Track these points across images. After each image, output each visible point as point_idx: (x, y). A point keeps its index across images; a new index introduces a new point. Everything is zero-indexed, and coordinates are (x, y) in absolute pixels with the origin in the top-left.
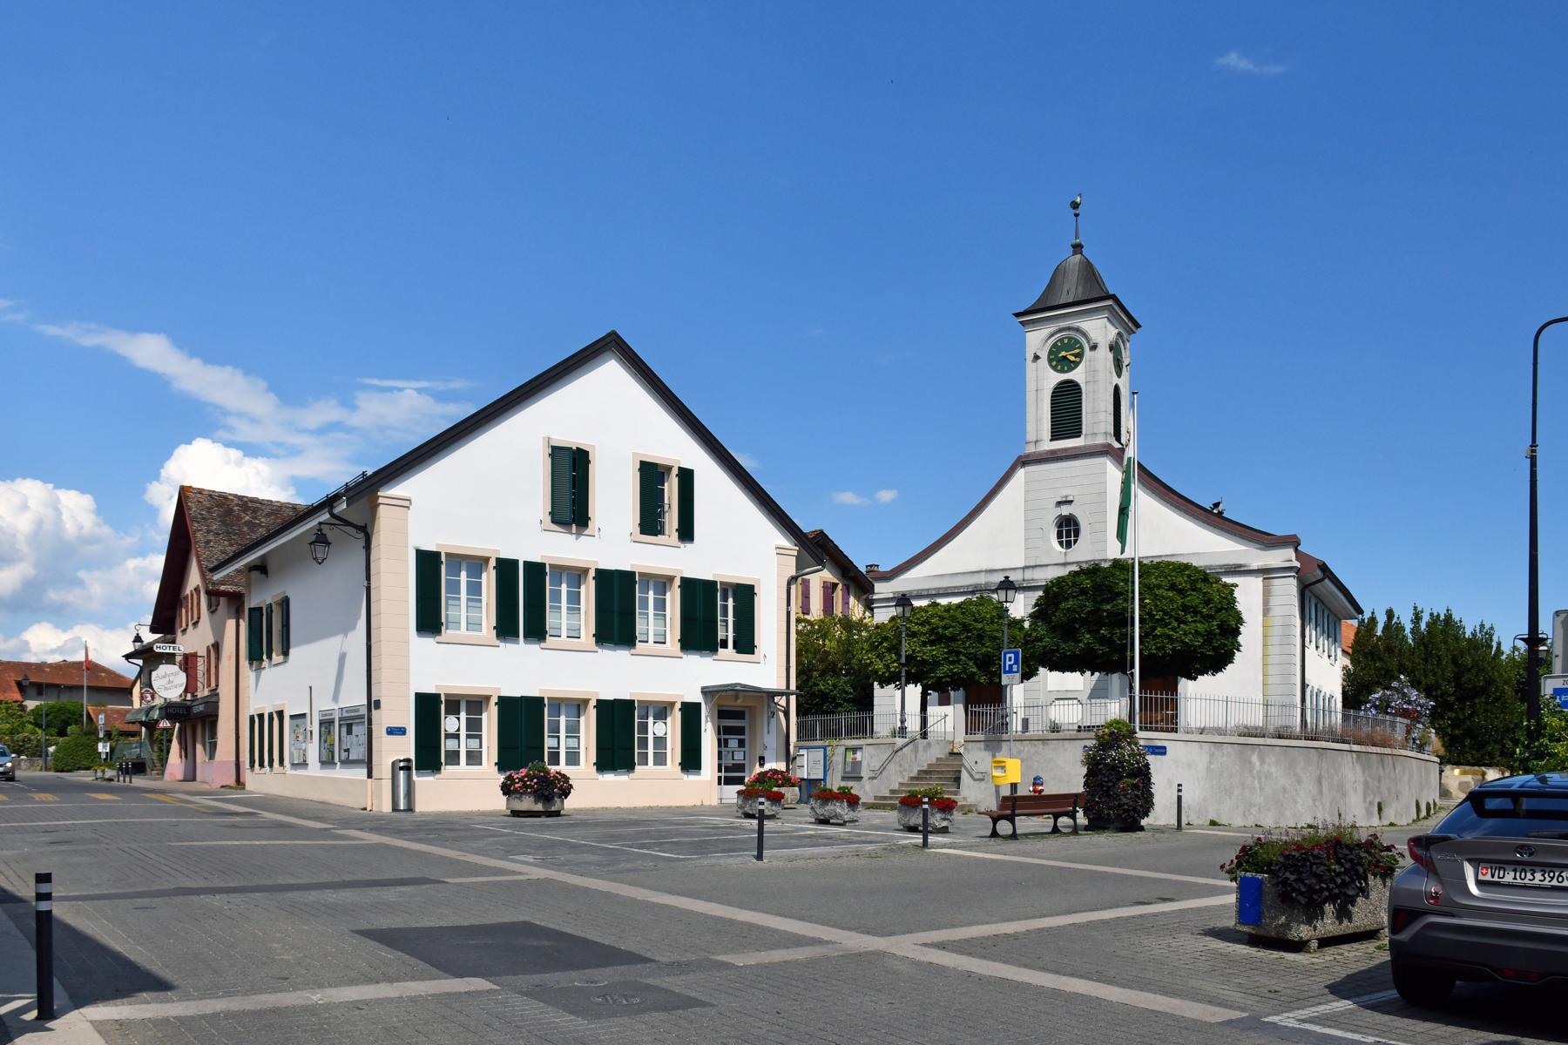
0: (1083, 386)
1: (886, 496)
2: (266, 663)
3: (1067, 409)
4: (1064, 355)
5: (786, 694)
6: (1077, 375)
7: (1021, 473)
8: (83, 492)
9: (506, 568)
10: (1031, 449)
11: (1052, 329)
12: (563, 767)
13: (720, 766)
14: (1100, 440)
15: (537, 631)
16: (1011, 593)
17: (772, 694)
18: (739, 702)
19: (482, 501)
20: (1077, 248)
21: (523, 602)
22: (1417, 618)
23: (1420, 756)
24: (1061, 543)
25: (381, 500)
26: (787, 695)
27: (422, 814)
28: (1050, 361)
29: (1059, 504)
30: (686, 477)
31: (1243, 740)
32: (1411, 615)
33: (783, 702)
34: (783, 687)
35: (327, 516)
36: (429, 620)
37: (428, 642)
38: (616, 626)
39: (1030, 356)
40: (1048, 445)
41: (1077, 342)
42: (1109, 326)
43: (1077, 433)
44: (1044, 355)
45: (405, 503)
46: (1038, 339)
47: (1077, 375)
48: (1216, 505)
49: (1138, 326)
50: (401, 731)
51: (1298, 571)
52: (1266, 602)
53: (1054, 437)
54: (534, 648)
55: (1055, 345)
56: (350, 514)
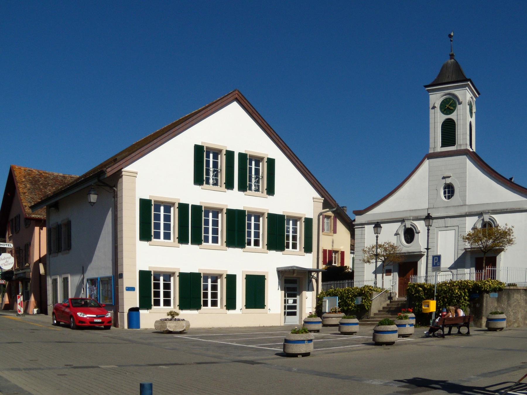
0: (456, 121)
1: (93, 198)
3: (449, 132)
4: (449, 105)
5: (317, 272)
7: (427, 162)
9: (183, 208)
10: (431, 151)
13: (285, 306)
14: (463, 148)
15: (197, 240)
16: (431, 221)
17: (310, 272)
18: (295, 275)
19: (161, 174)
20: (452, 56)
21: (192, 225)
24: (445, 197)
25: (123, 173)
26: (317, 272)
27: (192, 329)
28: (441, 108)
29: (444, 178)
30: (271, 163)
33: (315, 276)
34: (315, 267)
35: (96, 180)
36: (146, 234)
37: (145, 243)
38: (237, 237)
39: (431, 106)
40: (439, 149)
43: (453, 143)
44: (438, 105)
45: (134, 174)
46: (436, 99)
48: (511, 179)
50: (133, 289)
53: (444, 145)
54: (196, 247)
55: (446, 99)
56: (105, 182)
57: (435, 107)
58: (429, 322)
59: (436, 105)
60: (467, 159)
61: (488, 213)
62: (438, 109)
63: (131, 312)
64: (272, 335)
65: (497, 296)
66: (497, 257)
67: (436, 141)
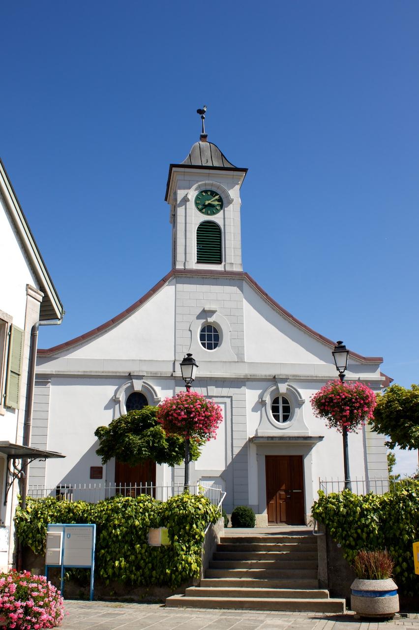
3: (210, 242)
4: (212, 201)
40: (193, 264)
53: (199, 261)
57: (188, 200)
58: (175, 433)
59: (189, 197)
60: (246, 306)
61: (284, 380)
62: (191, 205)
63: (352, 608)
64: (277, 528)
65: (165, 466)
66: (306, 461)
67: (188, 254)
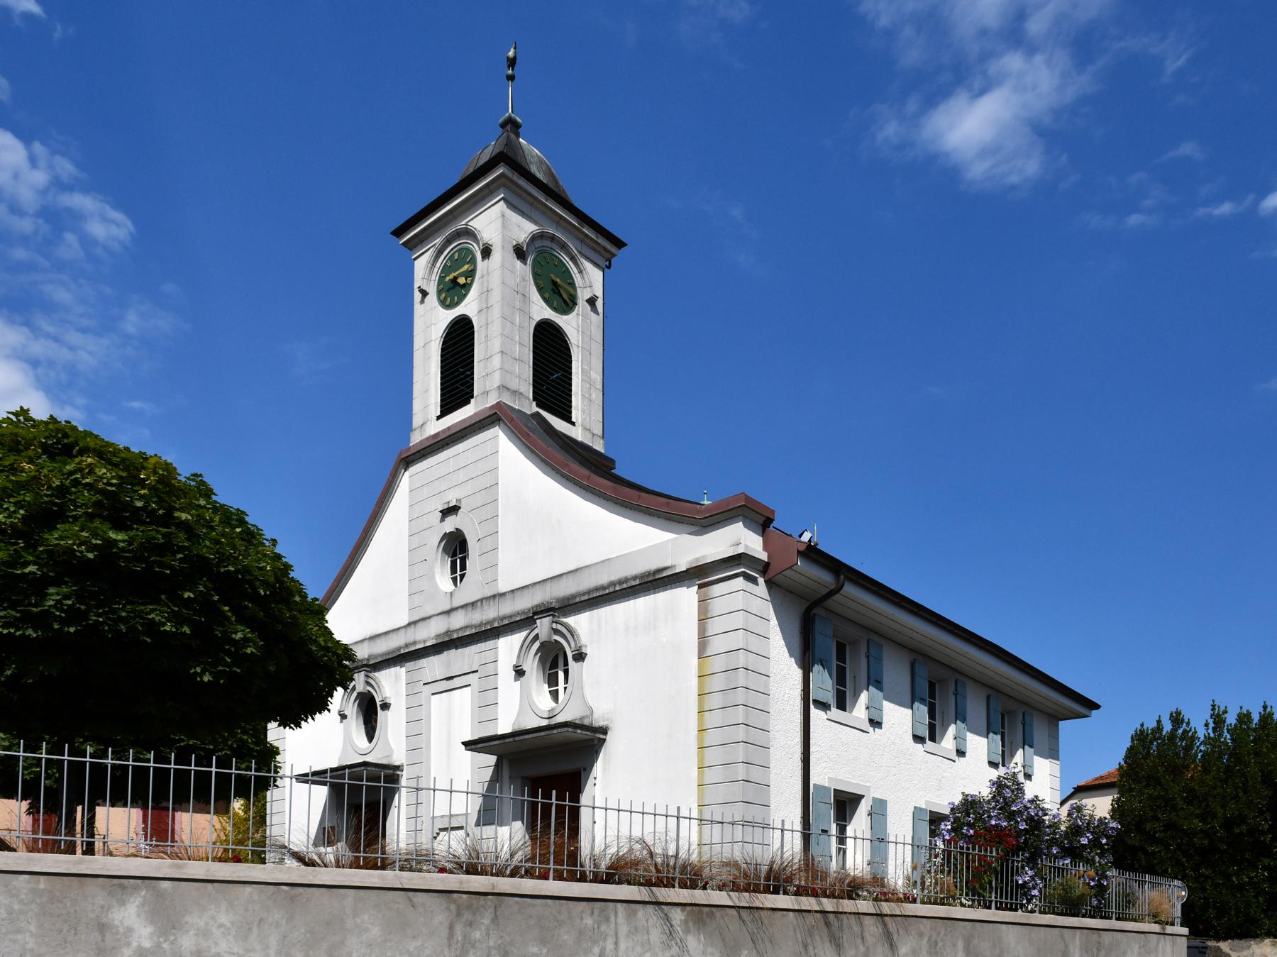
2: (764, 869)
6: (468, 307)
7: (406, 481)
8: (266, 730)
11: (438, 241)
12: (213, 950)
22: (1218, 720)
23: (1019, 916)
31: (745, 899)
32: (1206, 715)
41: (467, 249)
42: (514, 217)
44: (432, 289)
47: (468, 307)
49: (620, 244)
51: (764, 568)
52: (703, 640)
